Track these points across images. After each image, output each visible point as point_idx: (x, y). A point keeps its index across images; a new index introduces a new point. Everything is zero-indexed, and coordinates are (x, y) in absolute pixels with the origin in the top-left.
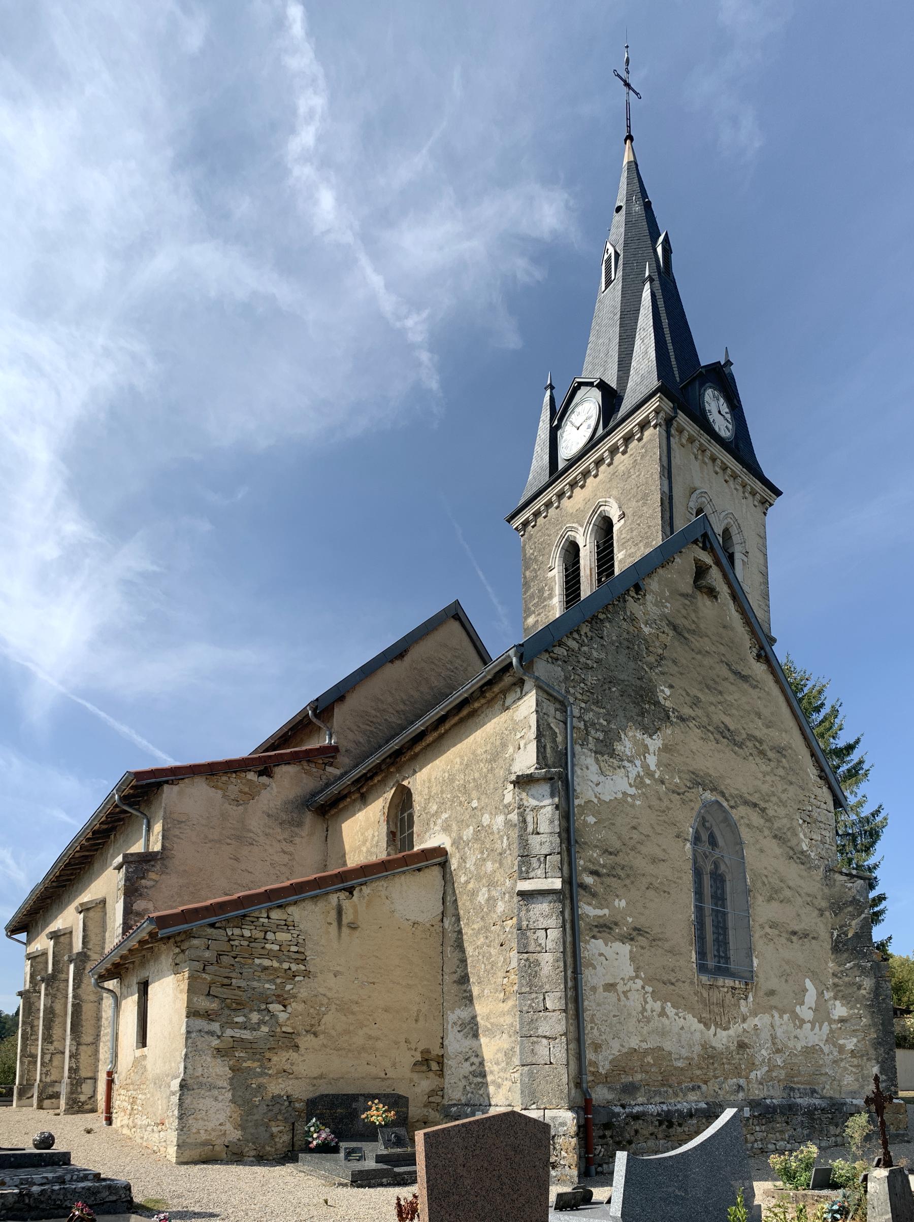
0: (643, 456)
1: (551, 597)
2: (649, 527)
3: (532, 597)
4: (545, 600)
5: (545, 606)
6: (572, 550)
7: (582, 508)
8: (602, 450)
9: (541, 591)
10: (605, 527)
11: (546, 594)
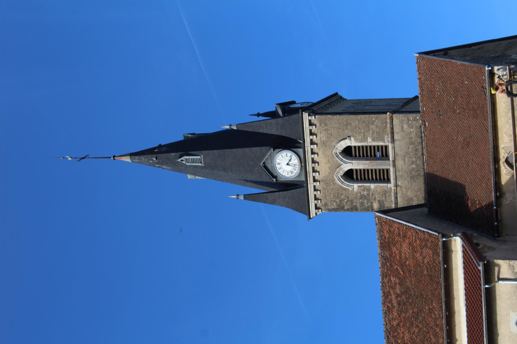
0: (326, 125)
1: (369, 189)
2: (364, 122)
3: (362, 204)
5: (372, 193)
6: (349, 175)
7: (330, 165)
8: (309, 157)
9: (362, 197)
10: (348, 152)
11: (366, 193)
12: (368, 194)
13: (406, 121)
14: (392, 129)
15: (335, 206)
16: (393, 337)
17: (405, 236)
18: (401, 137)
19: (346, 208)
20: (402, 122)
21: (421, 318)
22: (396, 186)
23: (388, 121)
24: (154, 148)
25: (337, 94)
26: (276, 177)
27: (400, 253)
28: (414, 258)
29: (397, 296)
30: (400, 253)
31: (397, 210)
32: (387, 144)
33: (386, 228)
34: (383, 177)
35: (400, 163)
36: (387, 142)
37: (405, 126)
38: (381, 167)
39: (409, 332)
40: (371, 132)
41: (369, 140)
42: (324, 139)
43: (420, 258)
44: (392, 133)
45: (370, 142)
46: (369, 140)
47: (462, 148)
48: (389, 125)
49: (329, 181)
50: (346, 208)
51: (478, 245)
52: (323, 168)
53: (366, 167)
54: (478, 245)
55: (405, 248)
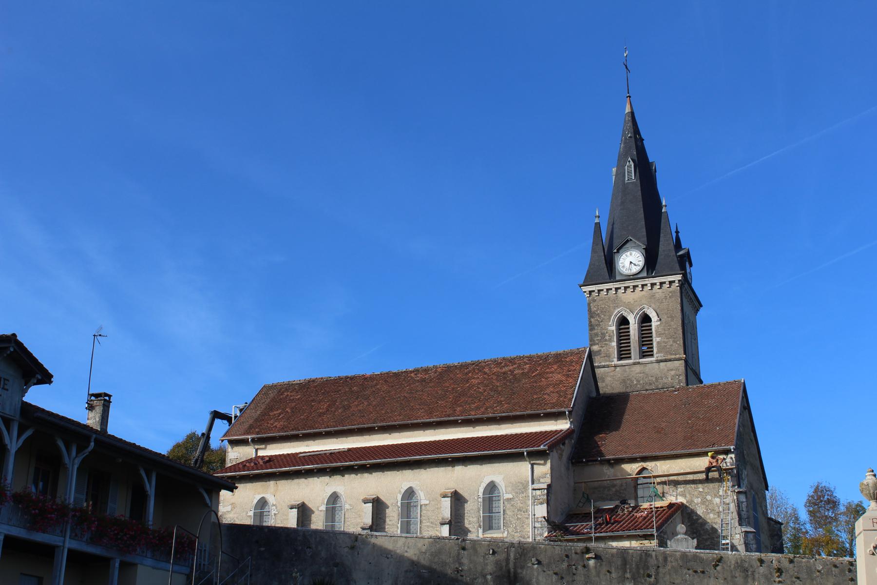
1: (611, 340)
3: (597, 335)
4: (606, 340)
6: (623, 322)
9: (603, 335)
10: (645, 319)
11: (607, 338)
12: (606, 340)
13: (678, 373)
14: (670, 360)
15: (594, 309)
16: (474, 369)
17: (568, 376)
18: (662, 369)
19: (592, 320)
20: (677, 369)
21: (492, 393)
22: (615, 366)
23: (678, 356)
24: (639, 134)
25: (701, 306)
26: (618, 252)
27: (552, 372)
28: (548, 386)
29: (512, 371)
30: (552, 372)
31: (593, 368)
32: (655, 356)
33: (575, 358)
34: (623, 353)
35: (637, 368)
36: (657, 356)
37: (673, 373)
38: (632, 351)
39: (479, 384)
40: (666, 340)
41: (658, 339)
42: (657, 296)
43: (548, 391)
44: (666, 361)
45: (656, 340)
46: (658, 339)
47: (655, 427)
48: (673, 357)
49: (616, 302)
50: (592, 320)
51: (564, 444)
52: (629, 297)
53: (632, 337)
54: (564, 444)
55: (558, 377)
